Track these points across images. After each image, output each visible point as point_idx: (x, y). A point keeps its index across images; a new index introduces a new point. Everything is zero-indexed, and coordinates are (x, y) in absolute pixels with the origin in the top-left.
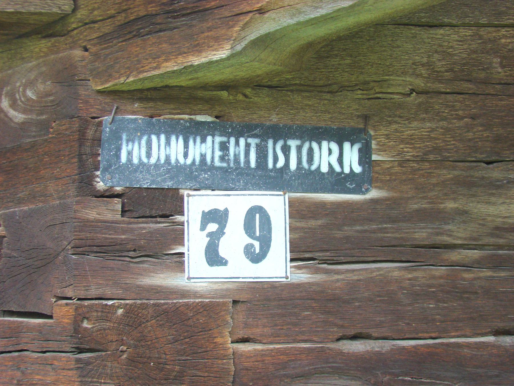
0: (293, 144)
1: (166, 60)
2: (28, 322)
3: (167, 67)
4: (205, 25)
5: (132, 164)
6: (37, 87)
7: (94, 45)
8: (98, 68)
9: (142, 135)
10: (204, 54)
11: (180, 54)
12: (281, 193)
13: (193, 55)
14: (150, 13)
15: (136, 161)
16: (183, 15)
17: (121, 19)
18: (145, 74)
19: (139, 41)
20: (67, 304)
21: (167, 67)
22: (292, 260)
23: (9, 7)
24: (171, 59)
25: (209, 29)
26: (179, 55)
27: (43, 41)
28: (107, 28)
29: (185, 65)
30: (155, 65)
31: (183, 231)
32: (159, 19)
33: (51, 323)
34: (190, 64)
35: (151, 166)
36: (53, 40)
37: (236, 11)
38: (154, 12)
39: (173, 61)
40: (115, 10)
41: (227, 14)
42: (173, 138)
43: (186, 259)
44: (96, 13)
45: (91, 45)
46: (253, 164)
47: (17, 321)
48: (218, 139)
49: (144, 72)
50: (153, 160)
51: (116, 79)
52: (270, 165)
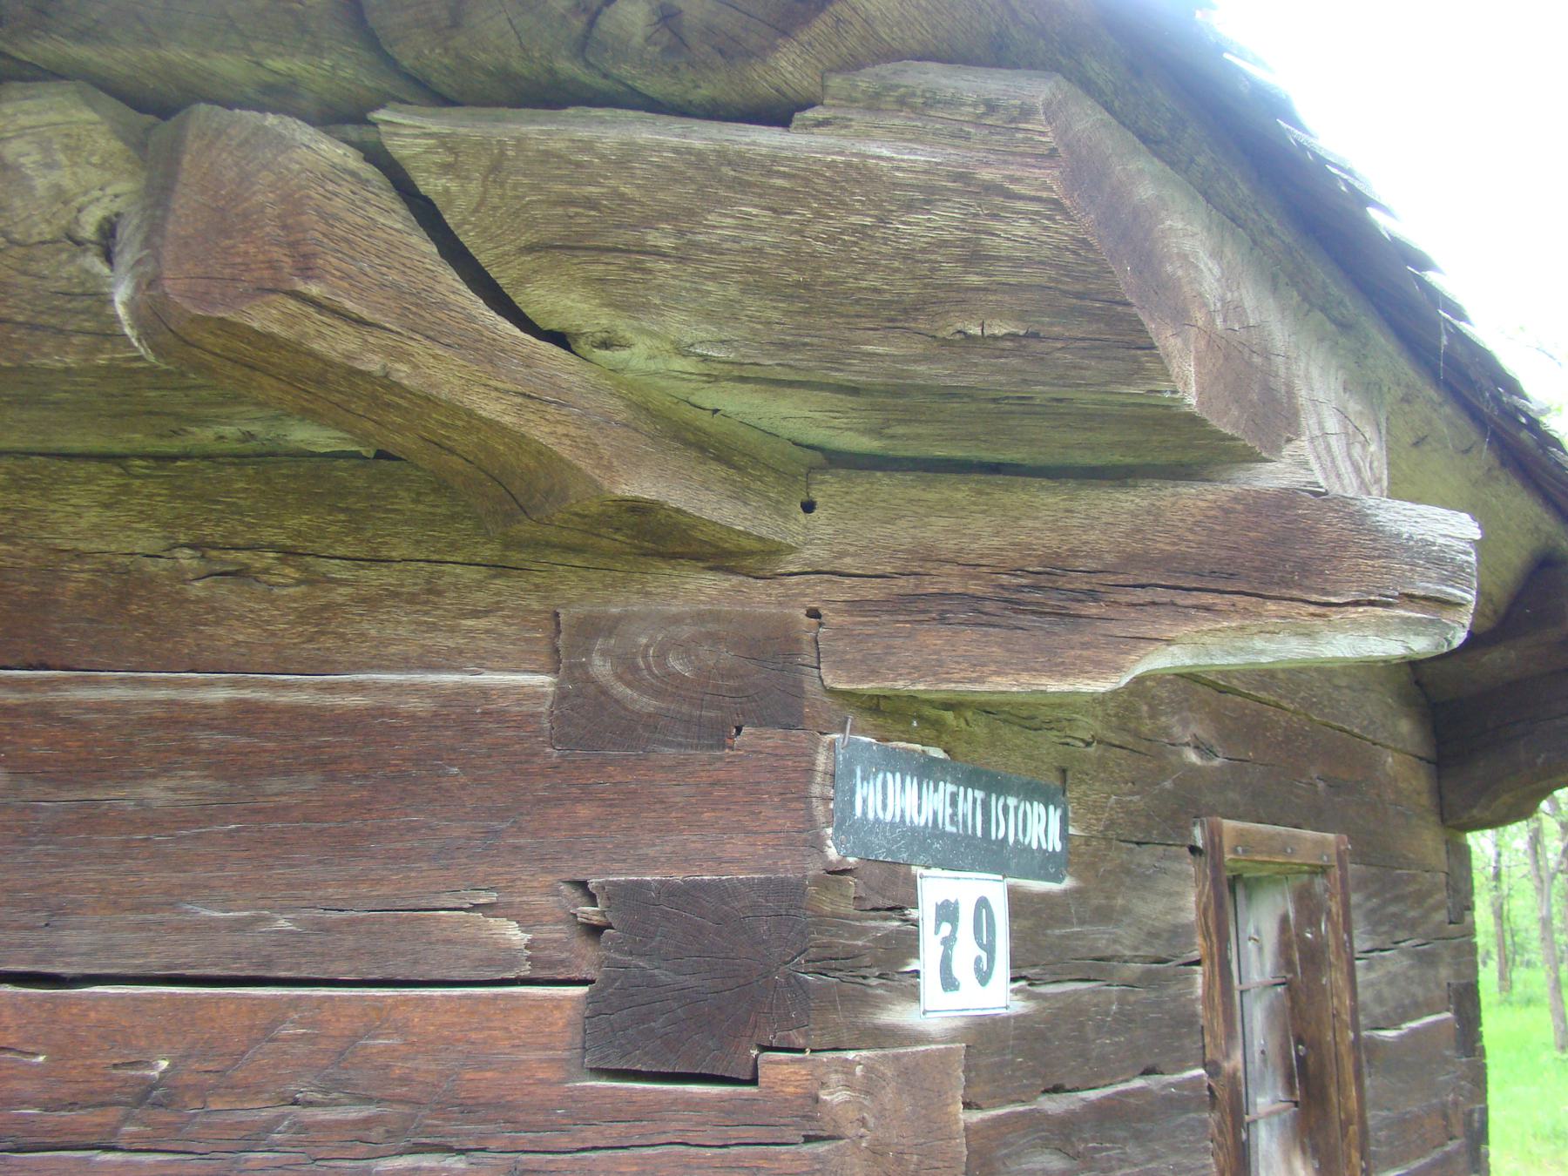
0: (1012, 801)
1: (998, 673)
2: (685, 1092)
3: (1000, 684)
4: (1076, 638)
5: (867, 820)
6: (697, 656)
7: (837, 612)
8: (845, 652)
9: (878, 771)
10: (1071, 680)
11: (1027, 670)
12: (1000, 877)
13: (1050, 677)
14: (970, 592)
15: (871, 816)
16: (1033, 612)
17: (905, 585)
18: (953, 685)
19: (945, 631)
20: (793, 1061)
21: (1000, 684)
22: (1013, 980)
23: (737, 522)
24: (1008, 674)
25: (1085, 646)
26: (1023, 670)
27: (709, 576)
28: (872, 590)
29: (1035, 688)
30: (974, 675)
31: (917, 934)
32: (989, 607)
33: (753, 1094)
34: (1043, 688)
35: (886, 824)
36: (735, 580)
37: (1133, 632)
38: (980, 594)
39: (1010, 677)
40: (894, 567)
41: (1117, 632)
42: (1035, 803)
43: (921, 981)
44: (848, 560)
45: (832, 610)
46: (979, 833)
47: (592, 1088)
48: (951, 788)
49: (950, 681)
50: (888, 818)
51: (886, 680)
52: (993, 837)
